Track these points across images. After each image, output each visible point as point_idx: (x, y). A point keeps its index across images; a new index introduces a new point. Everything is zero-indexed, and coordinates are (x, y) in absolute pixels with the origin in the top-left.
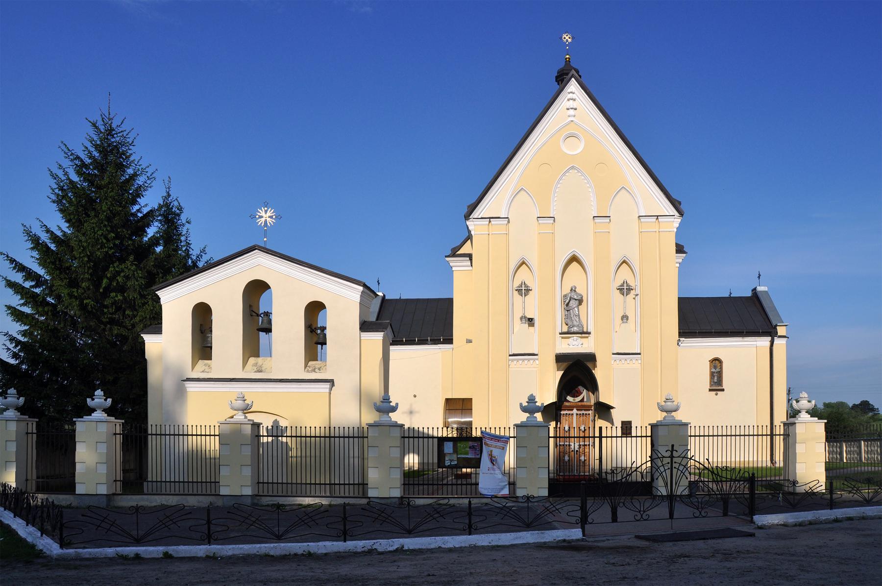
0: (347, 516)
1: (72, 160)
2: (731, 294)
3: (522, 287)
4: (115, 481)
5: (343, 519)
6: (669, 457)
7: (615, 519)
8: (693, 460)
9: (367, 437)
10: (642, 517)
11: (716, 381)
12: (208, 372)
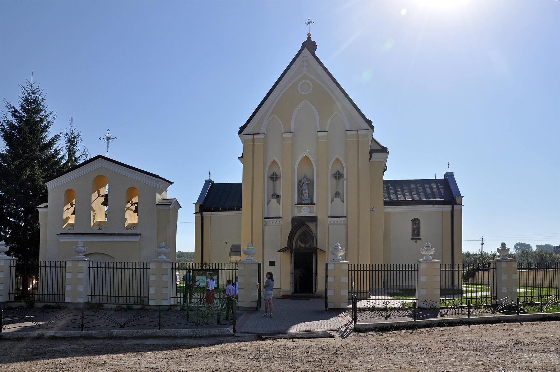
0: (84, 315)
1: (9, 109)
4: (89, 295)
9: (441, 270)
11: (416, 233)
12: (72, 230)
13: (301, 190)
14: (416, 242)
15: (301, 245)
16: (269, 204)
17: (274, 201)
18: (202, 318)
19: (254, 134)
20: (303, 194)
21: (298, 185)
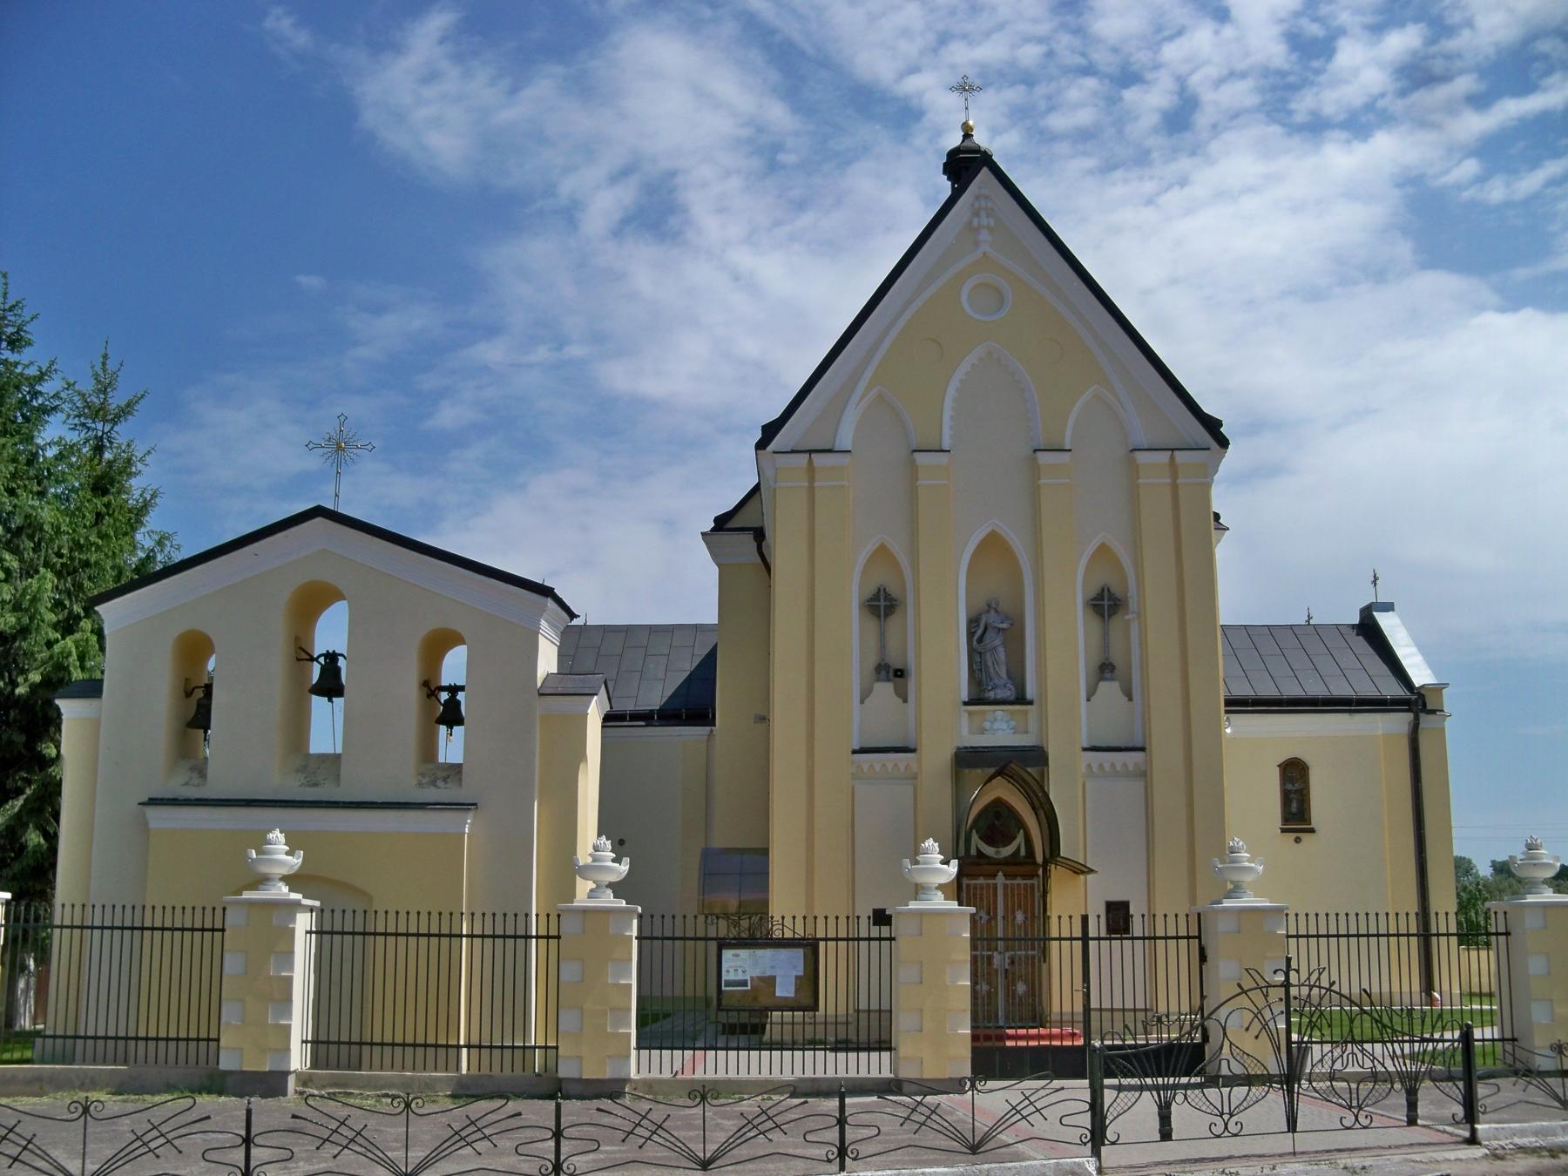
2: (1310, 618)
3: (879, 601)
5: (244, 1140)
6: (1281, 986)
7: (1292, 1125)
8: (1325, 988)
10: (1226, 1128)
13: (980, 654)
14: (1300, 840)
15: (982, 850)
16: (866, 701)
17: (885, 689)
18: (1221, 1115)
19: (810, 452)
20: (986, 665)
21: (970, 634)
